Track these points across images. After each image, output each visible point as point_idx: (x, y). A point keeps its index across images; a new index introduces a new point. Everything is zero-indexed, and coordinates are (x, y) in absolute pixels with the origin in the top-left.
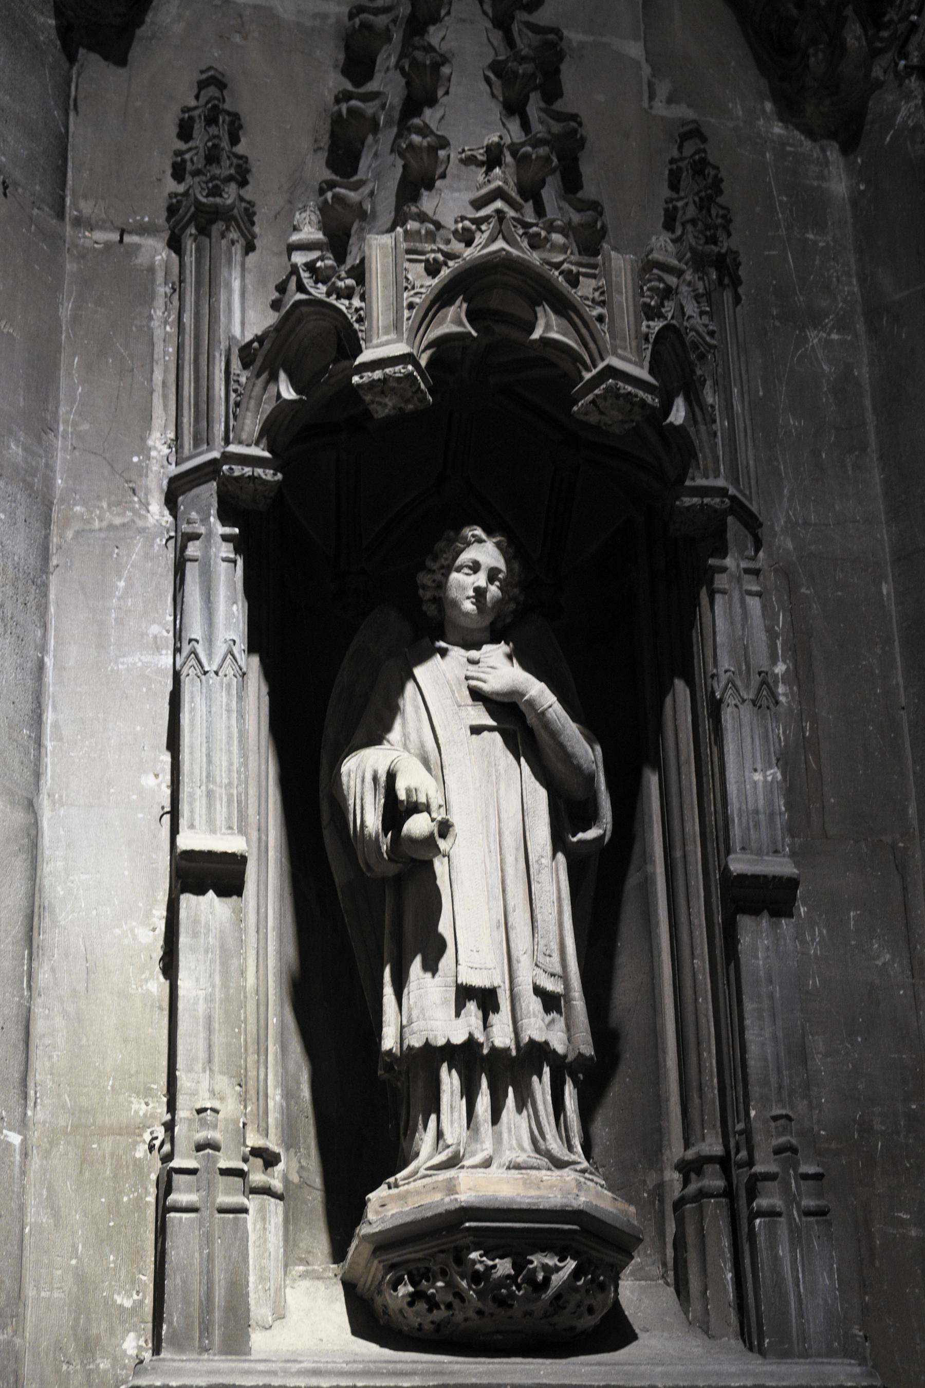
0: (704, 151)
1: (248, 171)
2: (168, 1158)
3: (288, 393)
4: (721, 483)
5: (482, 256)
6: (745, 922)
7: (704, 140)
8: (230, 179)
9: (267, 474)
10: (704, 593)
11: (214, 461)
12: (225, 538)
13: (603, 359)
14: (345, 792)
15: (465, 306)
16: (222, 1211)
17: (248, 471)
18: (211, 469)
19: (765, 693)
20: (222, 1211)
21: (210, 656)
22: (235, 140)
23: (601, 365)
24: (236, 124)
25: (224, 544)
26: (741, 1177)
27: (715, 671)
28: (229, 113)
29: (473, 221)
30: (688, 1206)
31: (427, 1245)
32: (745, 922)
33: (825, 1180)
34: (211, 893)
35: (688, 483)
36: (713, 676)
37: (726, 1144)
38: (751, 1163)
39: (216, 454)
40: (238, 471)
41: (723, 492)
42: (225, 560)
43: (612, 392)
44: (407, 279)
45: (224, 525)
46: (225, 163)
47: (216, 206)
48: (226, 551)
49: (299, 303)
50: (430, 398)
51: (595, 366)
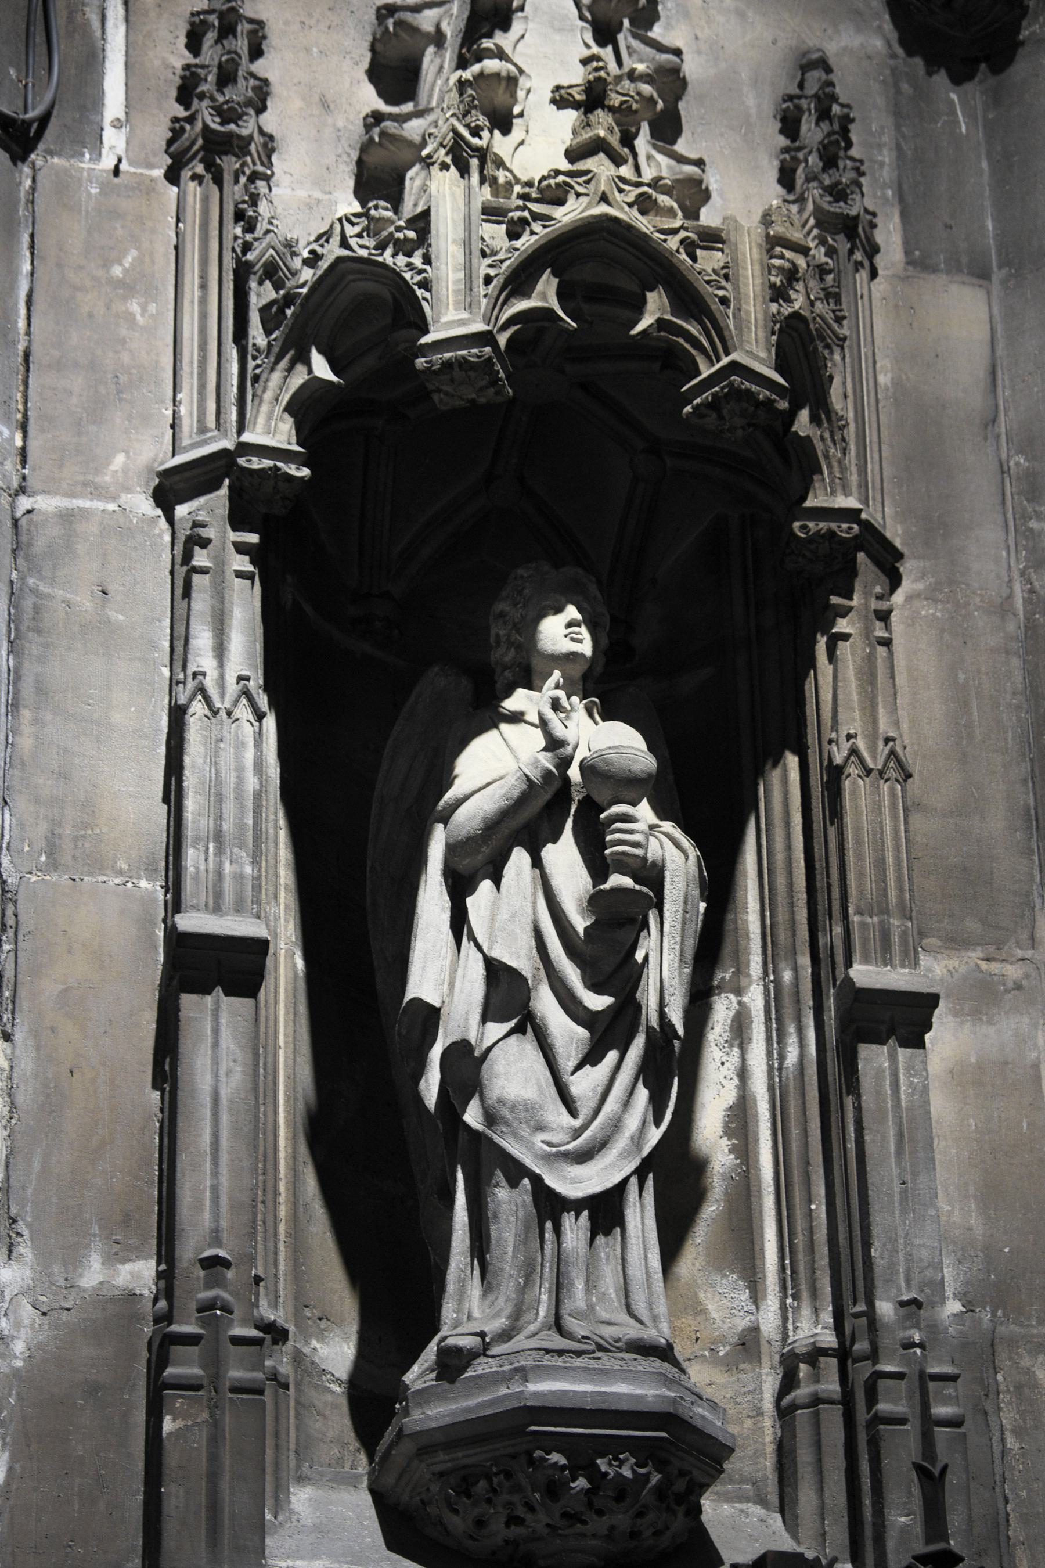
0: (831, 84)
1: (267, 94)
2: (167, 1318)
3: (321, 368)
4: (851, 502)
5: (581, 219)
6: (865, 1051)
7: (828, 70)
8: (249, 103)
9: (295, 471)
10: (822, 642)
11: (224, 452)
12: (241, 548)
13: (727, 354)
14: (651, 1108)
15: (555, 281)
16: (234, 1390)
17: (268, 463)
18: (222, 462)
19: (892, 764)
20: (234, 1390)
21: (222, 695)
22: (256, 52)
23: (725, 360)
24: (260, 34)
25: (238, 556)
26: (862, 1372)
27: (834, 735)
28: (251, 21)
29: (570, 174)
30: (799, 1412)
31: (485, 1449)
32: (865, 1051)
33: (959, 1381)
34: (218, 991)
35: (809, 503)
36: (830, 742)
37: (839, 1327)
38: (874, 1355)
39: (229, 444)
40: (257, 463)
41: (852, 515)
42: (240, 575)
43: (737, 394)
44: (483, 239)
45: (234, 530)
46: (241, 82)
47: (231, 135)
48: (243, 563)
49: (339, 260)
50: (510, 390)
51: (718, 360)
